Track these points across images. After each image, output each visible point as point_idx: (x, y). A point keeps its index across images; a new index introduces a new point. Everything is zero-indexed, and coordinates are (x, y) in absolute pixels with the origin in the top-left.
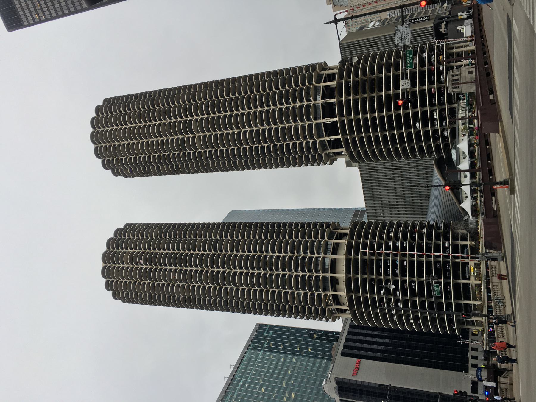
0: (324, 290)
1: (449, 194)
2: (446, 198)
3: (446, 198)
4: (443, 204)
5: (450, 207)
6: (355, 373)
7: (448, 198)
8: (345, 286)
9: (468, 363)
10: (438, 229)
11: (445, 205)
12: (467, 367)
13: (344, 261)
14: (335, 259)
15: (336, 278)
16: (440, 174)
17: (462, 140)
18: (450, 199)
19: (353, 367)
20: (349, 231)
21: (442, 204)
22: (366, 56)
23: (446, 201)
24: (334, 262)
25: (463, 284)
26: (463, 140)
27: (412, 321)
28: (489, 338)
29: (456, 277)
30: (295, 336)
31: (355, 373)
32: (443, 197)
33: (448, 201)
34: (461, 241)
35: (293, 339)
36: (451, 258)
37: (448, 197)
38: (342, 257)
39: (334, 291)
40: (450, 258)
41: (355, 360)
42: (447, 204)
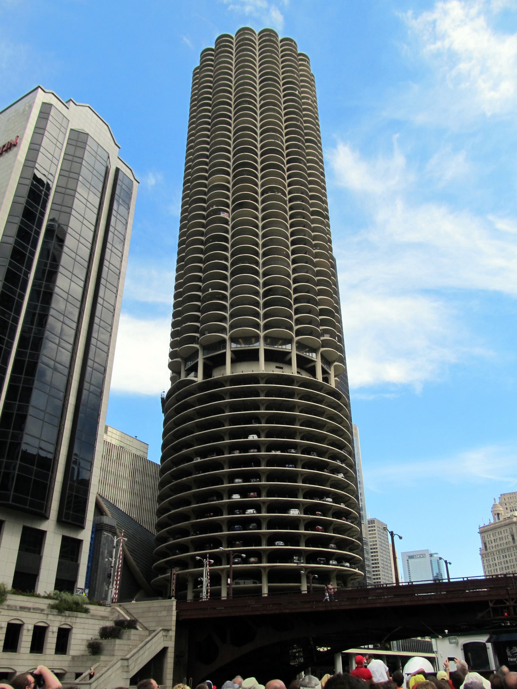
13: (290, 373)
38: (293, 371)
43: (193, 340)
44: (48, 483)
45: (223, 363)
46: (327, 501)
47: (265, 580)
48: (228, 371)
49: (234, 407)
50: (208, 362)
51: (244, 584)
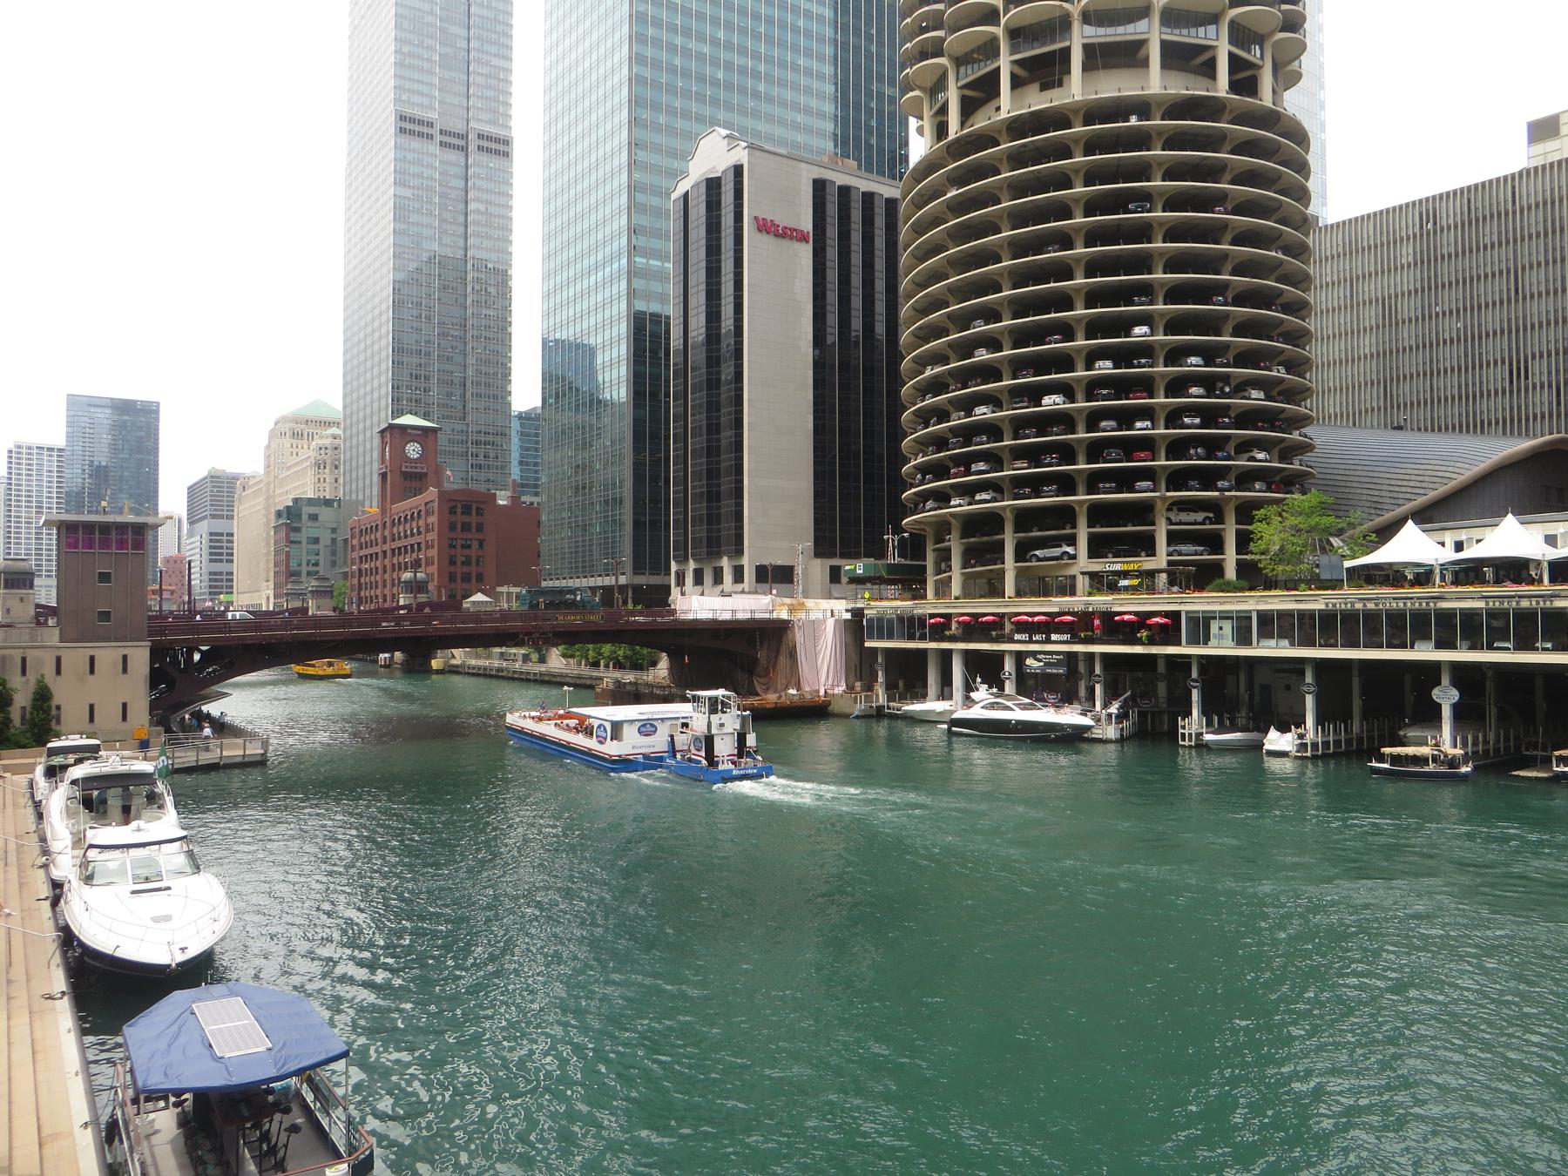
0: (1015, 34)
1: (1422, 491)
2: (1405, 483)
3: (1405, 483)
4: (1376, 475)
5: (1365, 498)
6: (764, 227)
7: (1404, 489)
8: (1033, 109)
9: (843, 556)
10: (1280, 451)
11: (1374, 480)
12: (832, 555)
13: (1136, 89)
14: (1145, 63)
15: (1065, 78)
16: (1511, 456)
17: (1441, 540)
18: (1401, 496)
19: (782, 219)
20: (1271, 105)
21: (1377, 469)
22: (1307, 457)
23: (1393, 482)
24: (1128, 55)
25: (1001, 545)
26: (1443, 544)
27: (929, 372)
28: (900, 619)
29: (1098, 514)
30: (881, 61)
31: (764, 227)
32: (1409, 472)
33: (1391, 488)
34: (1238, 532)
35: (869, 53)
36: (1169, 494)
37: (1409, 490)
38: (1155, 82)
39: (1013, 77)
40: (1168, 491)
41: (807, 225)
42: (1379, 487)
43: (936, 49)
44: (923, 697)
45: (995, 93)
46: (1191, 365)
47: (1082, 522)
48: (1007, 105)
49: (1019, 189)
50: (1020, 72)
51: (498, 147)
